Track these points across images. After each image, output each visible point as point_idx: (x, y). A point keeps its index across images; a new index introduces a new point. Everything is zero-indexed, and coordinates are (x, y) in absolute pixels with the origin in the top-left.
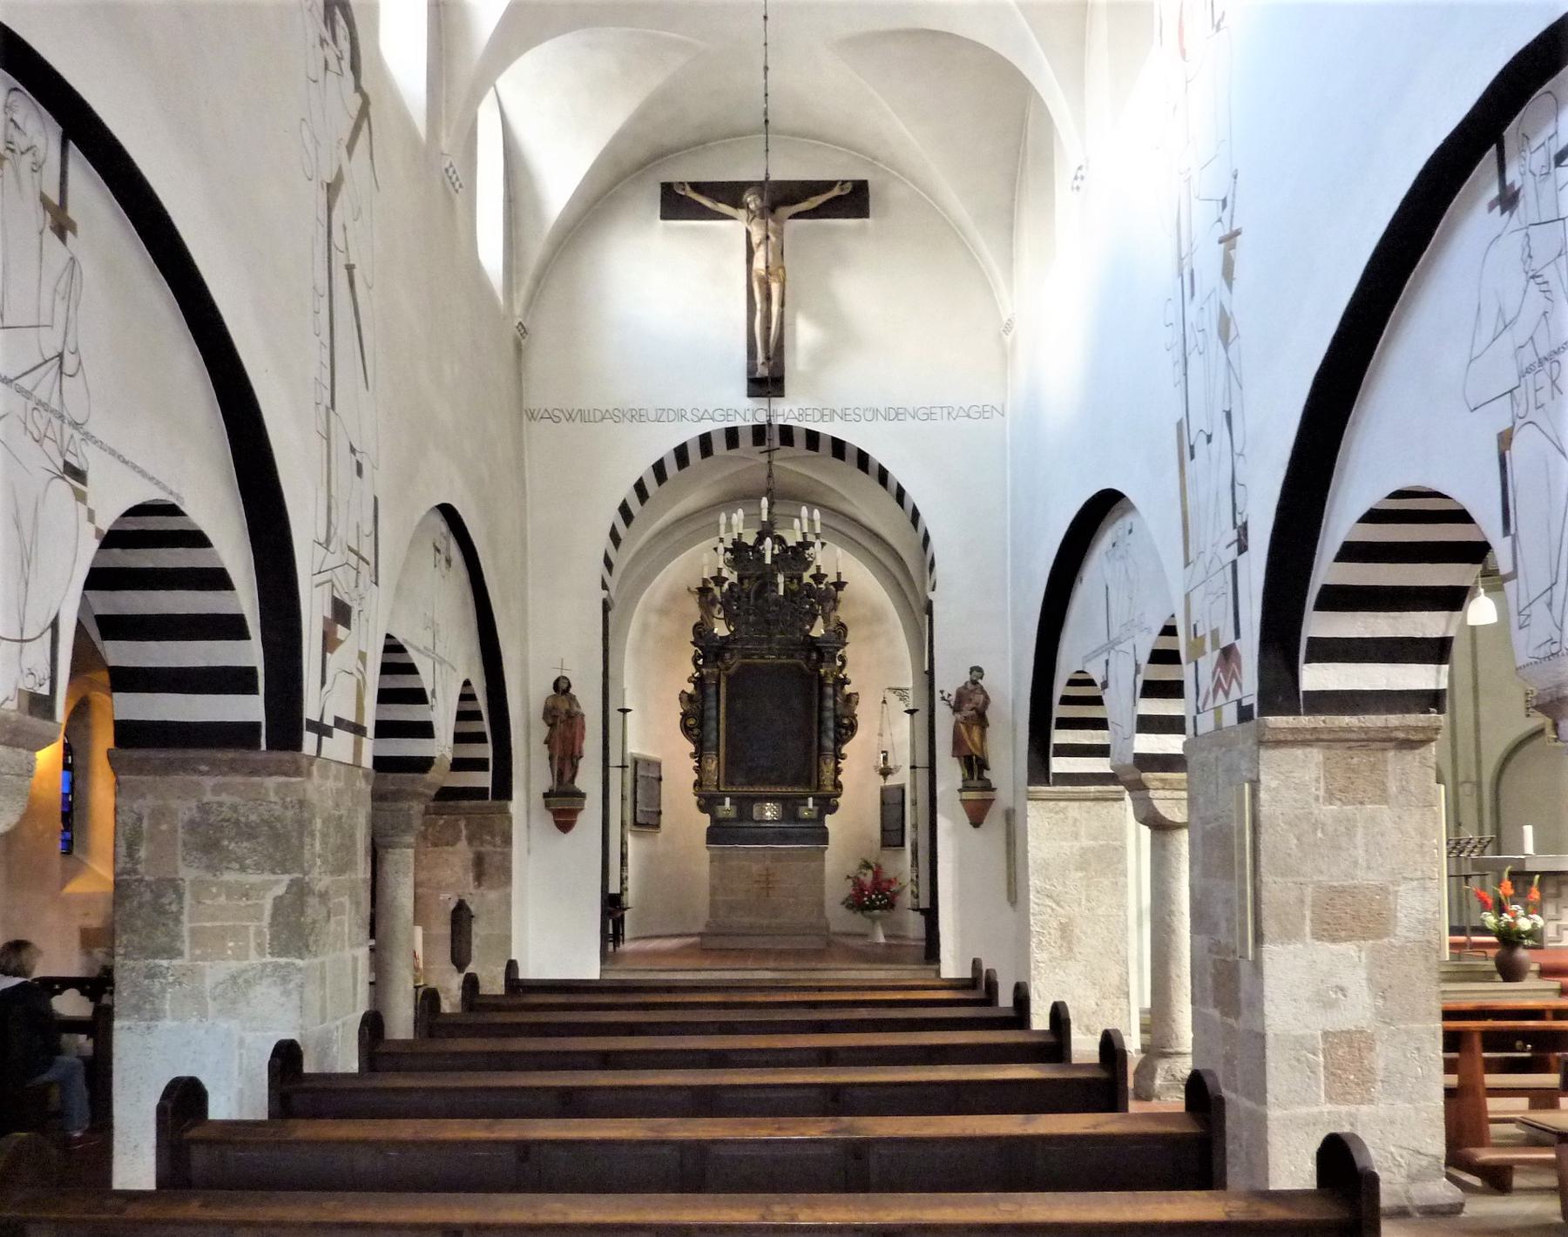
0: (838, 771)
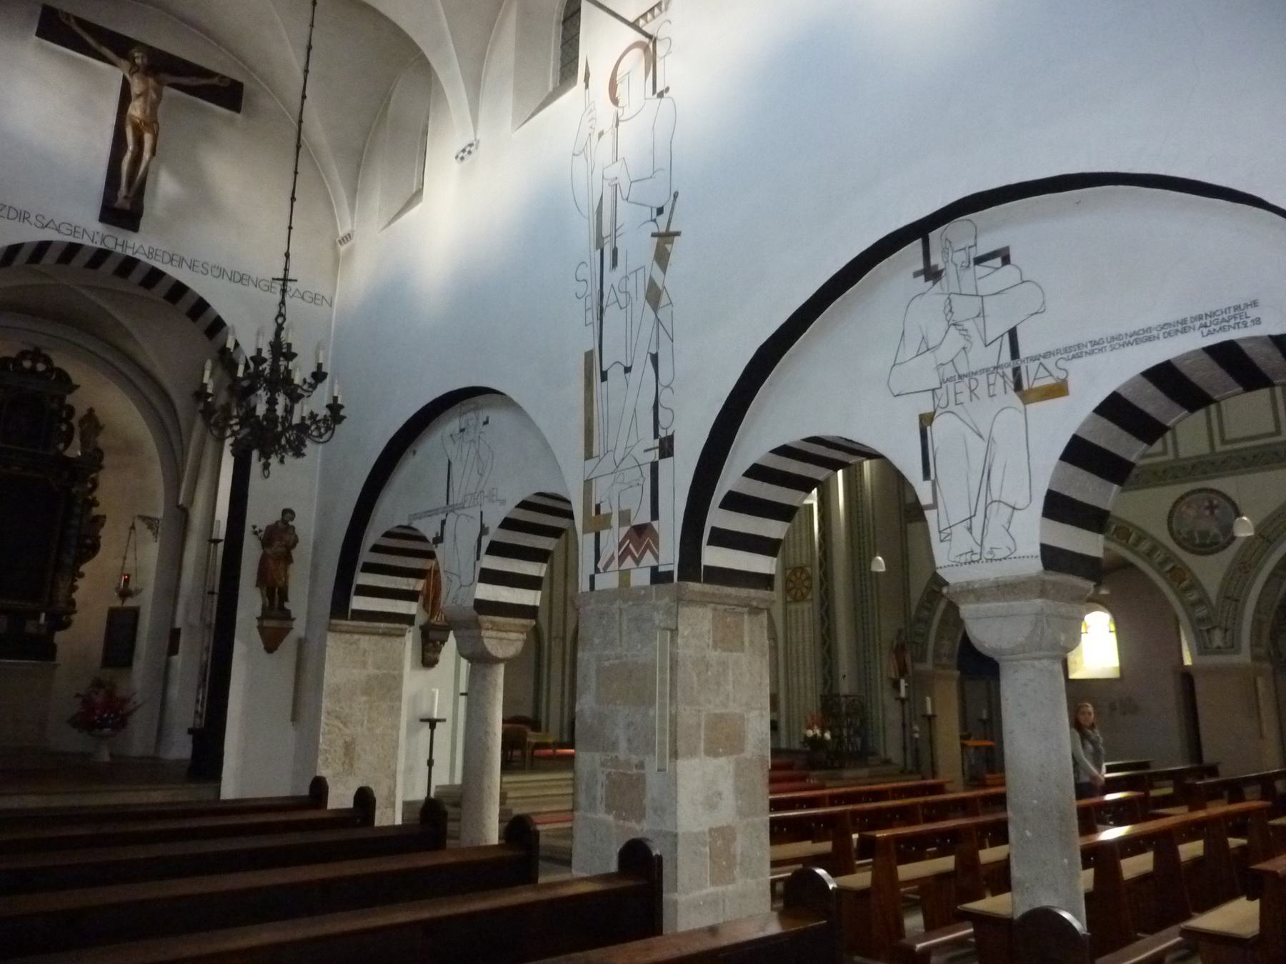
0: (73, 589)
